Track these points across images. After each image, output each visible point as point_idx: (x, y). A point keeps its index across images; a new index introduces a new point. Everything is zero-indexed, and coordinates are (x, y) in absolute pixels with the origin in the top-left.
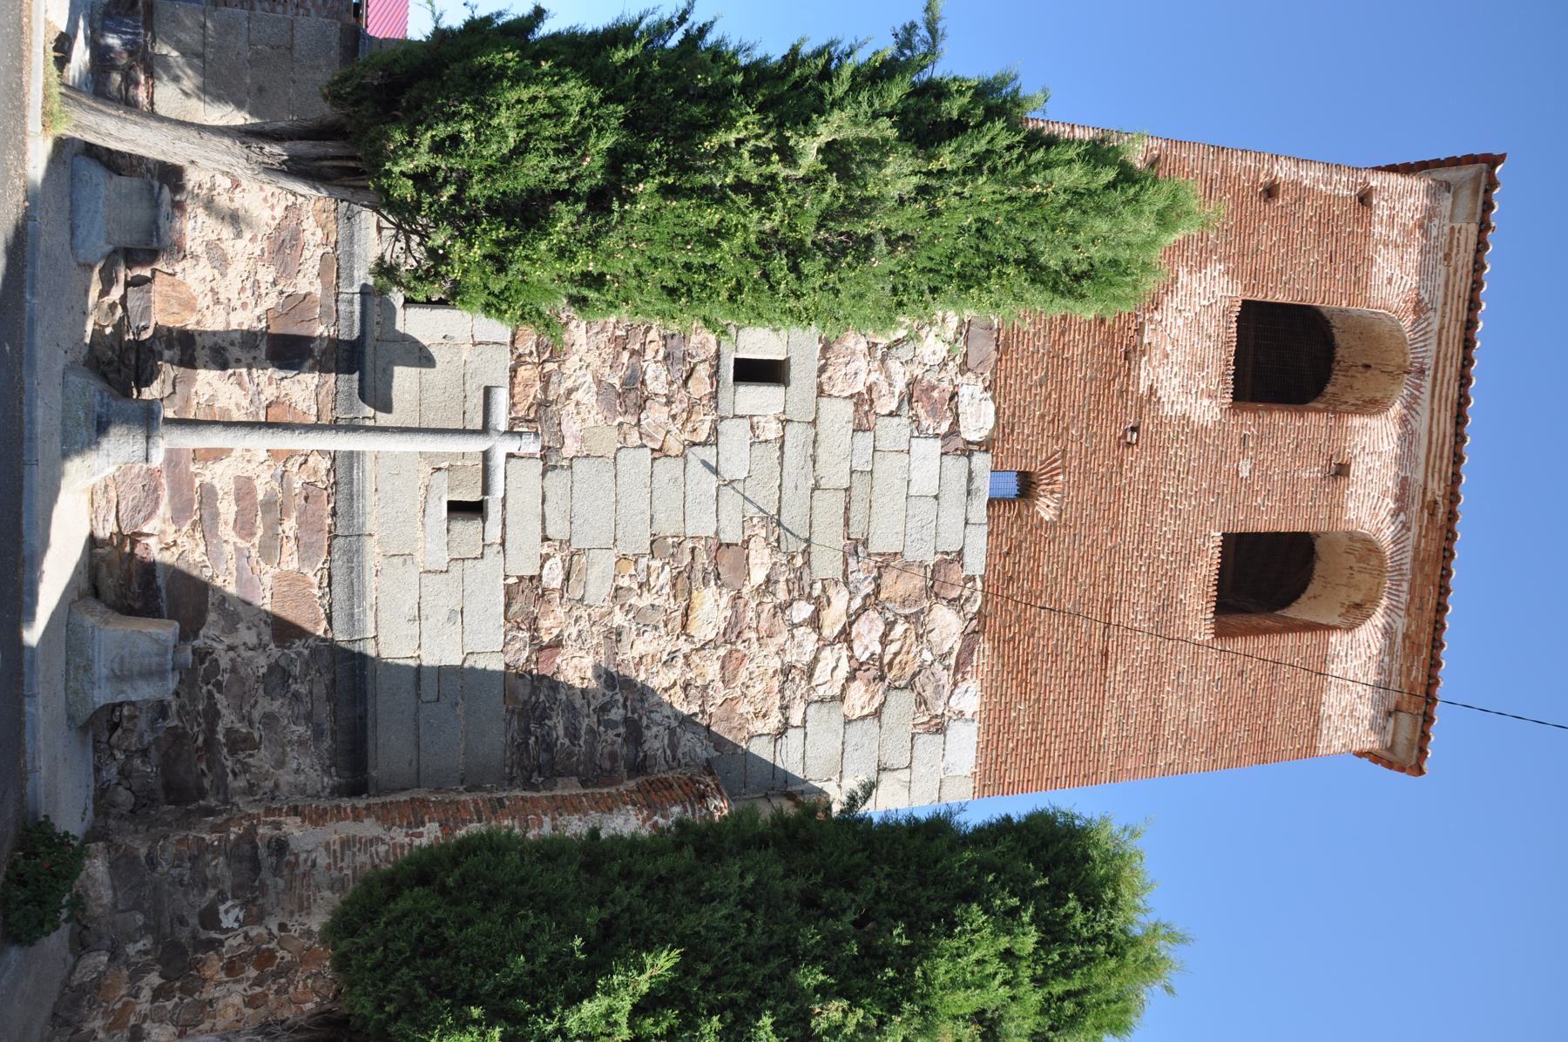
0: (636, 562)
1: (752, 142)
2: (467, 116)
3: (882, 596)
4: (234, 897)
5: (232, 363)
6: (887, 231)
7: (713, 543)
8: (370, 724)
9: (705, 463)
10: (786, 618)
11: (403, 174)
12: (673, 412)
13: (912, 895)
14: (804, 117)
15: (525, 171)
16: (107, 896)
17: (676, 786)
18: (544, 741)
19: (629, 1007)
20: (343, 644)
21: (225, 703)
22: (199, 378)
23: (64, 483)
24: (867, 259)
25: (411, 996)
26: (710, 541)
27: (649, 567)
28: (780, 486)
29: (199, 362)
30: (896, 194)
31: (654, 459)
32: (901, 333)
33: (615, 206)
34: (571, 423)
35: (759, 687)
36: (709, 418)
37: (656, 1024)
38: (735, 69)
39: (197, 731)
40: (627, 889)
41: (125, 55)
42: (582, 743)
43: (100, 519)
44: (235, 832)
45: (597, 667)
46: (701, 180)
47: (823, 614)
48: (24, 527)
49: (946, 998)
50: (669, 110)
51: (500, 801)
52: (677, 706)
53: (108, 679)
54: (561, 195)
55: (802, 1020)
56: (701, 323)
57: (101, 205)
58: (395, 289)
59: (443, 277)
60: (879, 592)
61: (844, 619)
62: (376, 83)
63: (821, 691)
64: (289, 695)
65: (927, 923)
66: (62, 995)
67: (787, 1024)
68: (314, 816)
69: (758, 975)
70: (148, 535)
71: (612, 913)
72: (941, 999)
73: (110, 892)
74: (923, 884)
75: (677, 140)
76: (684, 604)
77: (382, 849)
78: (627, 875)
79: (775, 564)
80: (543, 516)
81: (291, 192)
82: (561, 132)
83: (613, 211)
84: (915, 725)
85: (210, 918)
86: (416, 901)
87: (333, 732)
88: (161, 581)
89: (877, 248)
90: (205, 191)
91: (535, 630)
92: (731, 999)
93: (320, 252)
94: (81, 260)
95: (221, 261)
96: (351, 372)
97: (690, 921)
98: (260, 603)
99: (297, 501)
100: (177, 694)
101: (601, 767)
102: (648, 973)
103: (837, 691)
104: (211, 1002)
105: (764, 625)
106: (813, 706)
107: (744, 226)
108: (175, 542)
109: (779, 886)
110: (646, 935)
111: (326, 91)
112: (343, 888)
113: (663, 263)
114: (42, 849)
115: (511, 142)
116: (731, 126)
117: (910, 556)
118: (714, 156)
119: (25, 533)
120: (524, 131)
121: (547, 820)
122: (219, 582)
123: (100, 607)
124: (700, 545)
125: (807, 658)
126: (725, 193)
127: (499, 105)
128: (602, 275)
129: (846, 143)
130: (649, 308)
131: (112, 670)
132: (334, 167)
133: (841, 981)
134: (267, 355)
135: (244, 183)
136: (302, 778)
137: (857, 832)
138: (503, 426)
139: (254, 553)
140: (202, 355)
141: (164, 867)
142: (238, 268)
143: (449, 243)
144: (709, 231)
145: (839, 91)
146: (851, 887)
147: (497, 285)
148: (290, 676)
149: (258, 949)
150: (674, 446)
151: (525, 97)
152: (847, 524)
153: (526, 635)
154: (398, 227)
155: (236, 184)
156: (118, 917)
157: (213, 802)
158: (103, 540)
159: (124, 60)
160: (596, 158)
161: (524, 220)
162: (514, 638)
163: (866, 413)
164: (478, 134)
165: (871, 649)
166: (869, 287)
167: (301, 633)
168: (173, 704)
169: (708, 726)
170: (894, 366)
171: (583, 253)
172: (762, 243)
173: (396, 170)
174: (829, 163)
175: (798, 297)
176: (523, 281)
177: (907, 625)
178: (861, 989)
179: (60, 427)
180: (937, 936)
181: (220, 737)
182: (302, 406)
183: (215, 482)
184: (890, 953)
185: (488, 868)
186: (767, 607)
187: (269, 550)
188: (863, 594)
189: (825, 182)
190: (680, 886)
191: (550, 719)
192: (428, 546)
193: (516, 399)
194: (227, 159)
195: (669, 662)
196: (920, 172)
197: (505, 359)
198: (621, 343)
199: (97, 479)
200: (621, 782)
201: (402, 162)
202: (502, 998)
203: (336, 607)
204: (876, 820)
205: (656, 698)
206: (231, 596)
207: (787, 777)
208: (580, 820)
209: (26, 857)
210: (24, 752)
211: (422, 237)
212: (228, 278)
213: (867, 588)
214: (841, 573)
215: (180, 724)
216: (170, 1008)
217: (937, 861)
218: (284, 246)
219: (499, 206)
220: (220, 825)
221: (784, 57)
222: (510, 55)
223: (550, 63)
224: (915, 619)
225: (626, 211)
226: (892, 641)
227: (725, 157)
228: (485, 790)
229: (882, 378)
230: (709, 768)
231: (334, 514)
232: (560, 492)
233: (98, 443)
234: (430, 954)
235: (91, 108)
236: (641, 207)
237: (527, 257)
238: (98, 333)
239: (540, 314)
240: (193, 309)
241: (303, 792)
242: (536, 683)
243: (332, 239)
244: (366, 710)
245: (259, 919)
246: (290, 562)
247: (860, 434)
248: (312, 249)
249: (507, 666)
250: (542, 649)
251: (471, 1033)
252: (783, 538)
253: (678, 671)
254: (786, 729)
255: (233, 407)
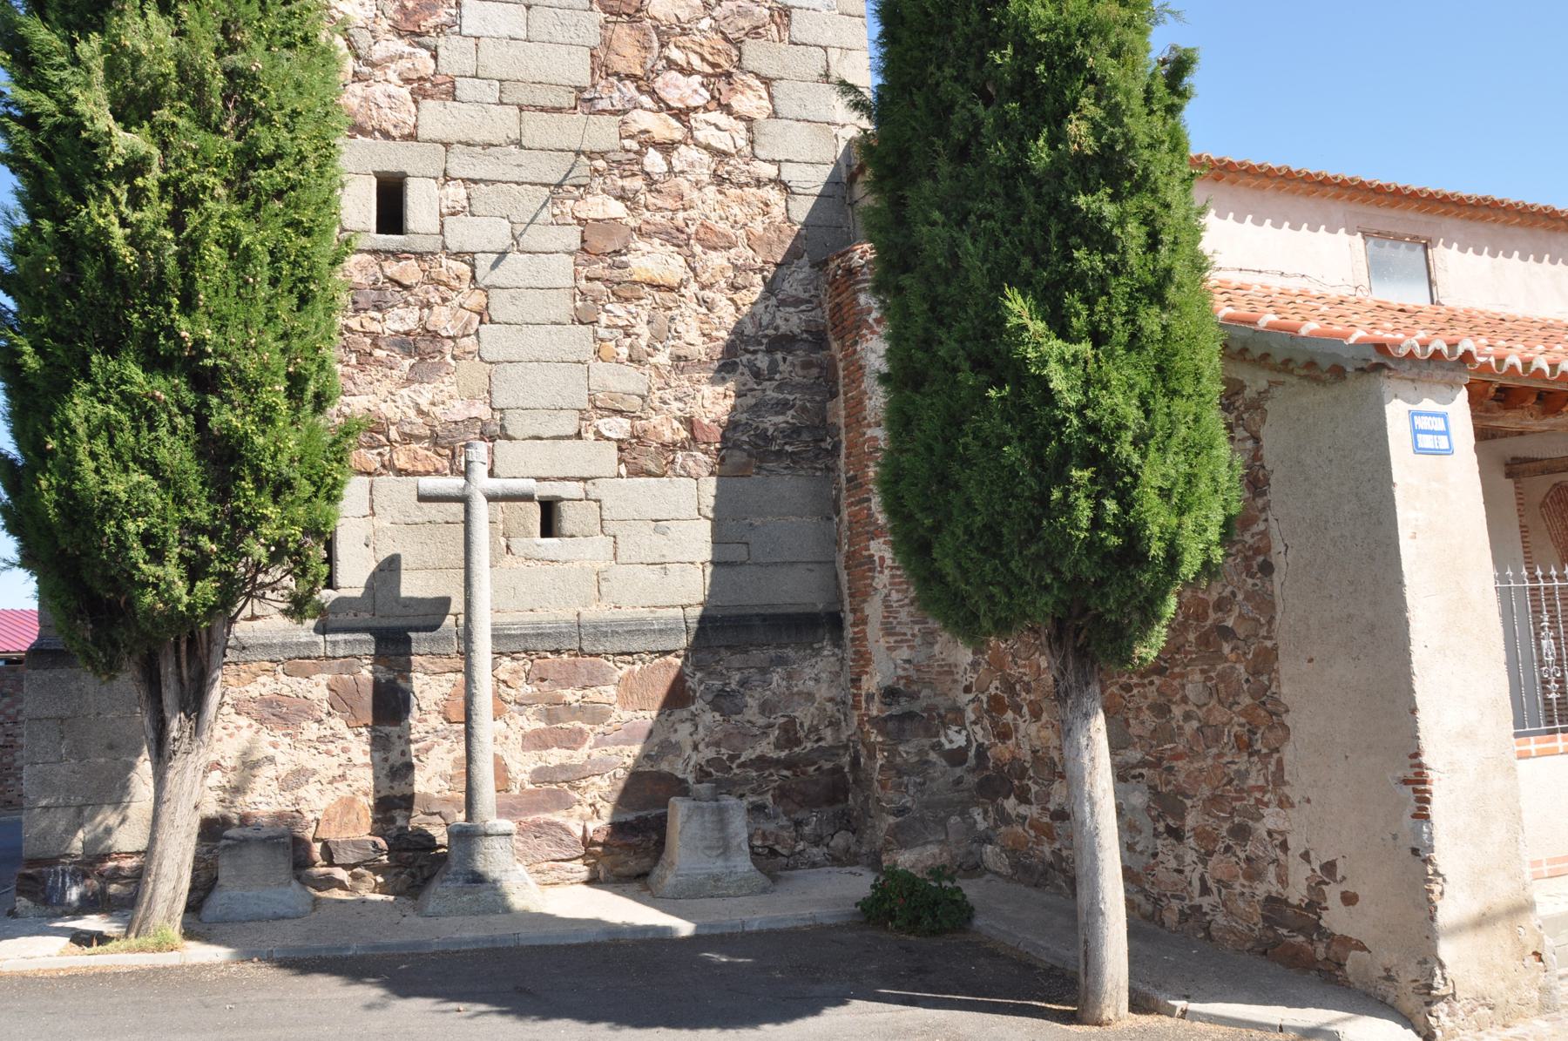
0: (602, 340)
1: (122, 208)
2: (119, 526)
3: (639, 72)
4: (937, 735)
5: (405, 759)
6: (219, 52)
7: (581, 258)
8: (771, 611)
9: (494, 266)
10: (662, 179)
11: (189, 592)
12: (439, 301)
13: (961, 42)
14: (87, 149)
15: (176, 462)
16: (933, 849)
17: (837, 300)
18: (789, 436)
19: (1060, 341)
20: (690, 639)
21: (750, 751)
22: (423, 790)
23: (534, 909)
24: (254, 78)
25: (1038, 557)
26: (579, 261)
27: (608, 327)
28: (517, 183)
29: (407, 791)
30: (171, 40)
31: (491, 321)
32: (339, 41)
33: (209, 362)
34: (455, 411)
35: (736, 210)
36: (444, 261)
37: (1078, 315)
38: (35, 229)
39: (777, 776)
40: (941, 343)
41: (88, 882)
42: (791, 398)
43: (570, 875)
44: (875, 737)
45: (713, 382)
46: (171, 266)
47: (658, 138)
48: (580, 941)
49: (1072, 9)
50: (92, 304)
51: (849, 480)
52: (755, 298)
53: (727, 860)
54: (201, 423)
55: (1083, 164)
56: (338, 268)
57: (250, 894)
58: (317, 597)
59: (301, 546)
60: (635, 76)
61: (664, 115)
62: (90, 626)
63: (741, 143)
64: (742, 690)
65: (991, 27)
66: (1019, 881)
67: (1087, 180)
68: (862, 662)
69: (1033, 208)
70: (585, 830)
71: (966, 359)
72: (1072, 14)
73: (929, 847)
74: (950, 29)
75: (127, 295)
76: (647, 289)
77: (895, 596)
78: (927, 343)
79: (603, 191)
80: (554, 438)
81: (219, 708)
82: (128, 424)
83: (216, 365)
84: (781, 41)
85: (956, 757)
86: (947, 555)
87: (779, 646)
88: (630, 817)
89: (240, 64)
90: (227, 796)
91: (675, 445)
92: (1058, 237)
93: (283, 678)
94: (309, 908)
95: (300, 776)
96: (409, 640)
97: (977, 278)
98: (650, 721)
99: (546, 689)
100: (742, 796)
101: (818, 378)
102: (1027, 321)
103: (742, 125)
104: (1034, 752)
105: (670, 203)
106: (758, 152)
107: (223, 217)
108: (590, 805)
109: (945, 185)
110: (988, 324)
111: (105, 678)
112: (932, 633)
113: (272, 309)
114: (886, 906)
115: (145, 478)
116: (105, 233)
117: (595, 40)
118: (143, 252)
119: (585, 940)
120: (131, 464)
121: (869, 433)
122: (630, 762)
123: (657, 871)
124: (584, 271)
125: (706, 157)
126: (186, 240)
127: (104, 492)
128: (289, 376)
129: (113, 98)
130: (323, 325)
131: (718, 856)
132: (188, 664)
133: (1045, 122)
134: (396, 725)
135: (213, 757)
136: (824, 675)
137: (892, 101)
138: (461, 481)
139: (600, 729)
140: (399, 789)
141: (907, 801)
142: (306, 758)
143: (262, 540)
144: (231, 258)
145: (49, 105)
146: (949, 109)
147: (306, 489)
148: (722, 690)
149: (987, 712)
150: (477, 299)
151: (92, 465)
152: (559, 110)
153: (680, 455)
154: (249, 596)
155: (217, 765)
156: (952, 838)
157: (846, 759)
158: (591, 872)
159: (94, 883)
160: (155, 384)
161: (231, 461)
162: (683, 467)
163: (434, 86)
164: (139, 514)
165: (697, 86)
166: (287, 75)
167: (679, 680)
168: (751, 800)
169: (777, 265)
170: (378, 52)
171: (265, 396)
172: (241, 197)
173: (185, 599)
174: (141, 118)
175: (304, 158)
176: (300, 461)
177: (671, 46)
178: (1056, 101)
179: (480, 917)
180: (1005, 15)
181: (783, 754)
182: (447, 688)
183: (529, 770)
184: (1020, 67)
185: (916, 485)
186: (651, 199)
187: (596, 714)
188: (636, 94)
189: (164, 124)
190: (941, 289)
191: (766, 430)
192: (588, 556)
193: (431, 469)
194: (189, 773)
195: (709, 306)
196: (141, 8)
197: (388, 481)
198: (364, 359)
199: (531, 881)
200: (833, 357)
201: (176, 593)
202: (1045, 469)
203: (653, 647)
204: (879, 81)
205: (747, 320)
206: (643, 749)
207: (832, 182)
208: (870, 399)
209: (893, 918)
210: (796, 928)
211: (258, 571)
212: (317, 768)
213: (630, 88)
214: (613, 118)
215: (771, 792)
216: (1037, 788)
217: (927, 14)
218: (278, 713)
219: (218, 489)
220: (868, 751)
221: (13, 171)
222: (44, 483)
223: (49, 439)
224: (663, 36)
225: (215, 351)
226: (689, 63)
227: (142, 240)
228: (838, 496)
229: (393, 66)
230: (820, 265)
231: (558, 652)
232: (528, 421)
233: (495, 881)
234: (997, 537)
235: (149, 907)
236: (208, 334)
237: (273, 457)
238: (382, 889)
239: (336, 442)
240: (353, 800)
241: (837, 674)
242: (730, 445)
243: (268, 665)
244: (757, 615)
245: (959, 712)
246: (609, 693)
247: (458, 93)
248: (279, 686)
249: (712, 474)
250: (694, 439)
251: (1077, 499)
252: (575, 181)
253: (718, 296)
254: (781, 181)
255: (452, 756)
